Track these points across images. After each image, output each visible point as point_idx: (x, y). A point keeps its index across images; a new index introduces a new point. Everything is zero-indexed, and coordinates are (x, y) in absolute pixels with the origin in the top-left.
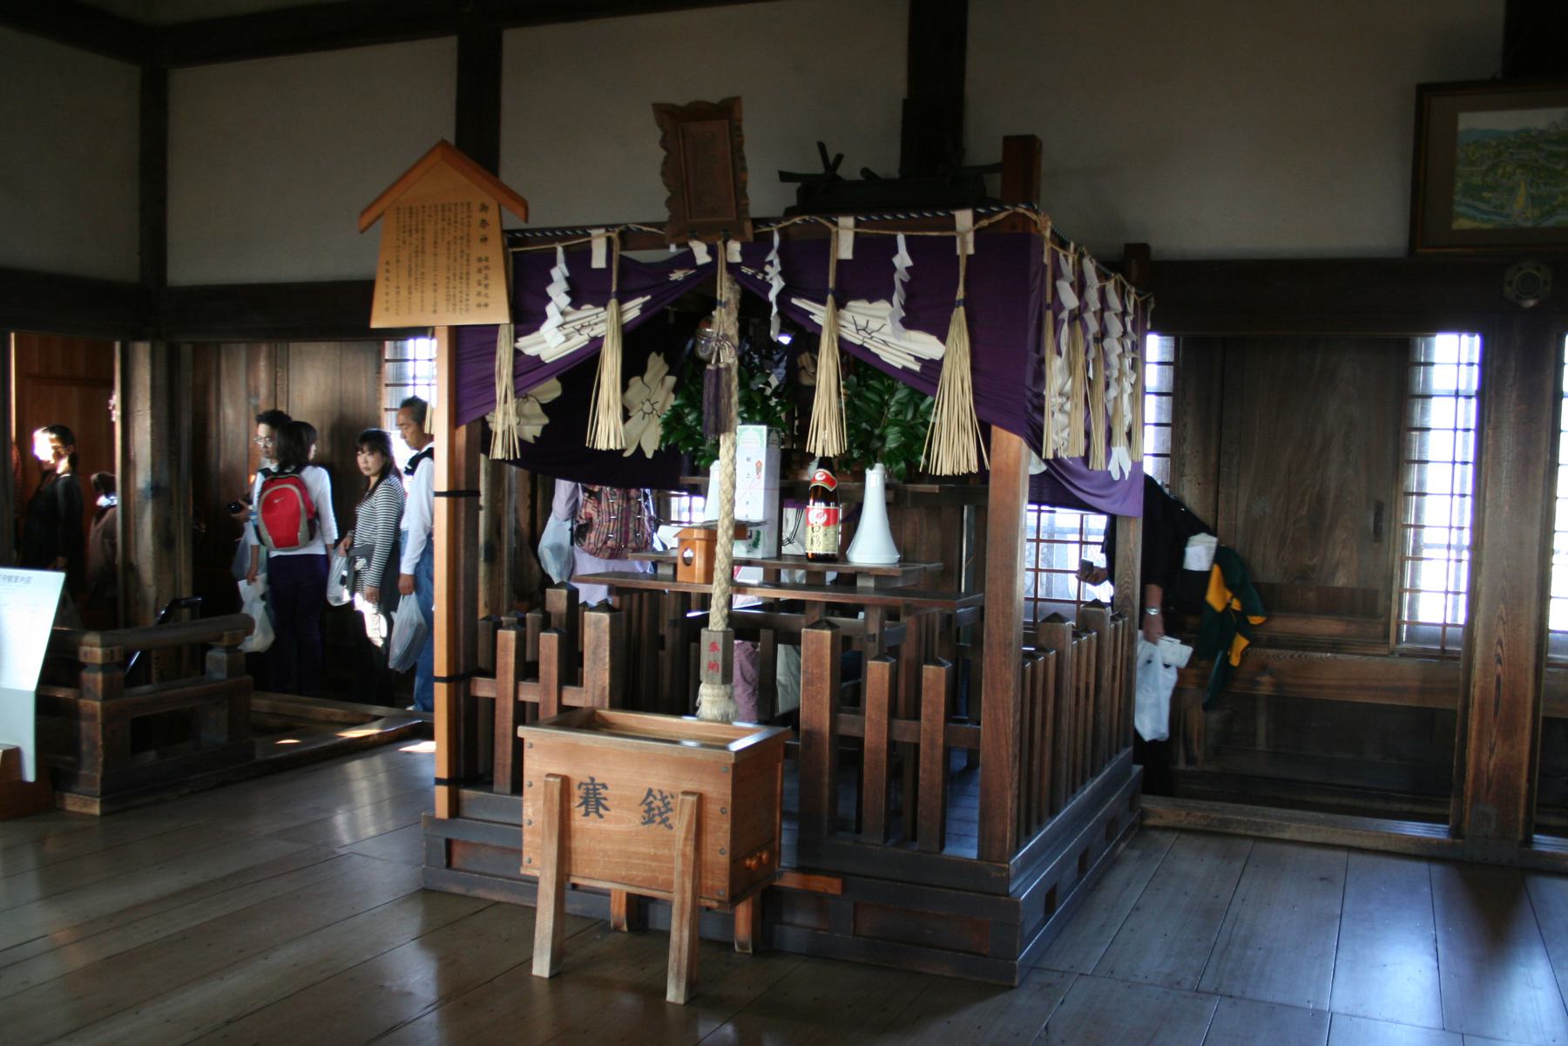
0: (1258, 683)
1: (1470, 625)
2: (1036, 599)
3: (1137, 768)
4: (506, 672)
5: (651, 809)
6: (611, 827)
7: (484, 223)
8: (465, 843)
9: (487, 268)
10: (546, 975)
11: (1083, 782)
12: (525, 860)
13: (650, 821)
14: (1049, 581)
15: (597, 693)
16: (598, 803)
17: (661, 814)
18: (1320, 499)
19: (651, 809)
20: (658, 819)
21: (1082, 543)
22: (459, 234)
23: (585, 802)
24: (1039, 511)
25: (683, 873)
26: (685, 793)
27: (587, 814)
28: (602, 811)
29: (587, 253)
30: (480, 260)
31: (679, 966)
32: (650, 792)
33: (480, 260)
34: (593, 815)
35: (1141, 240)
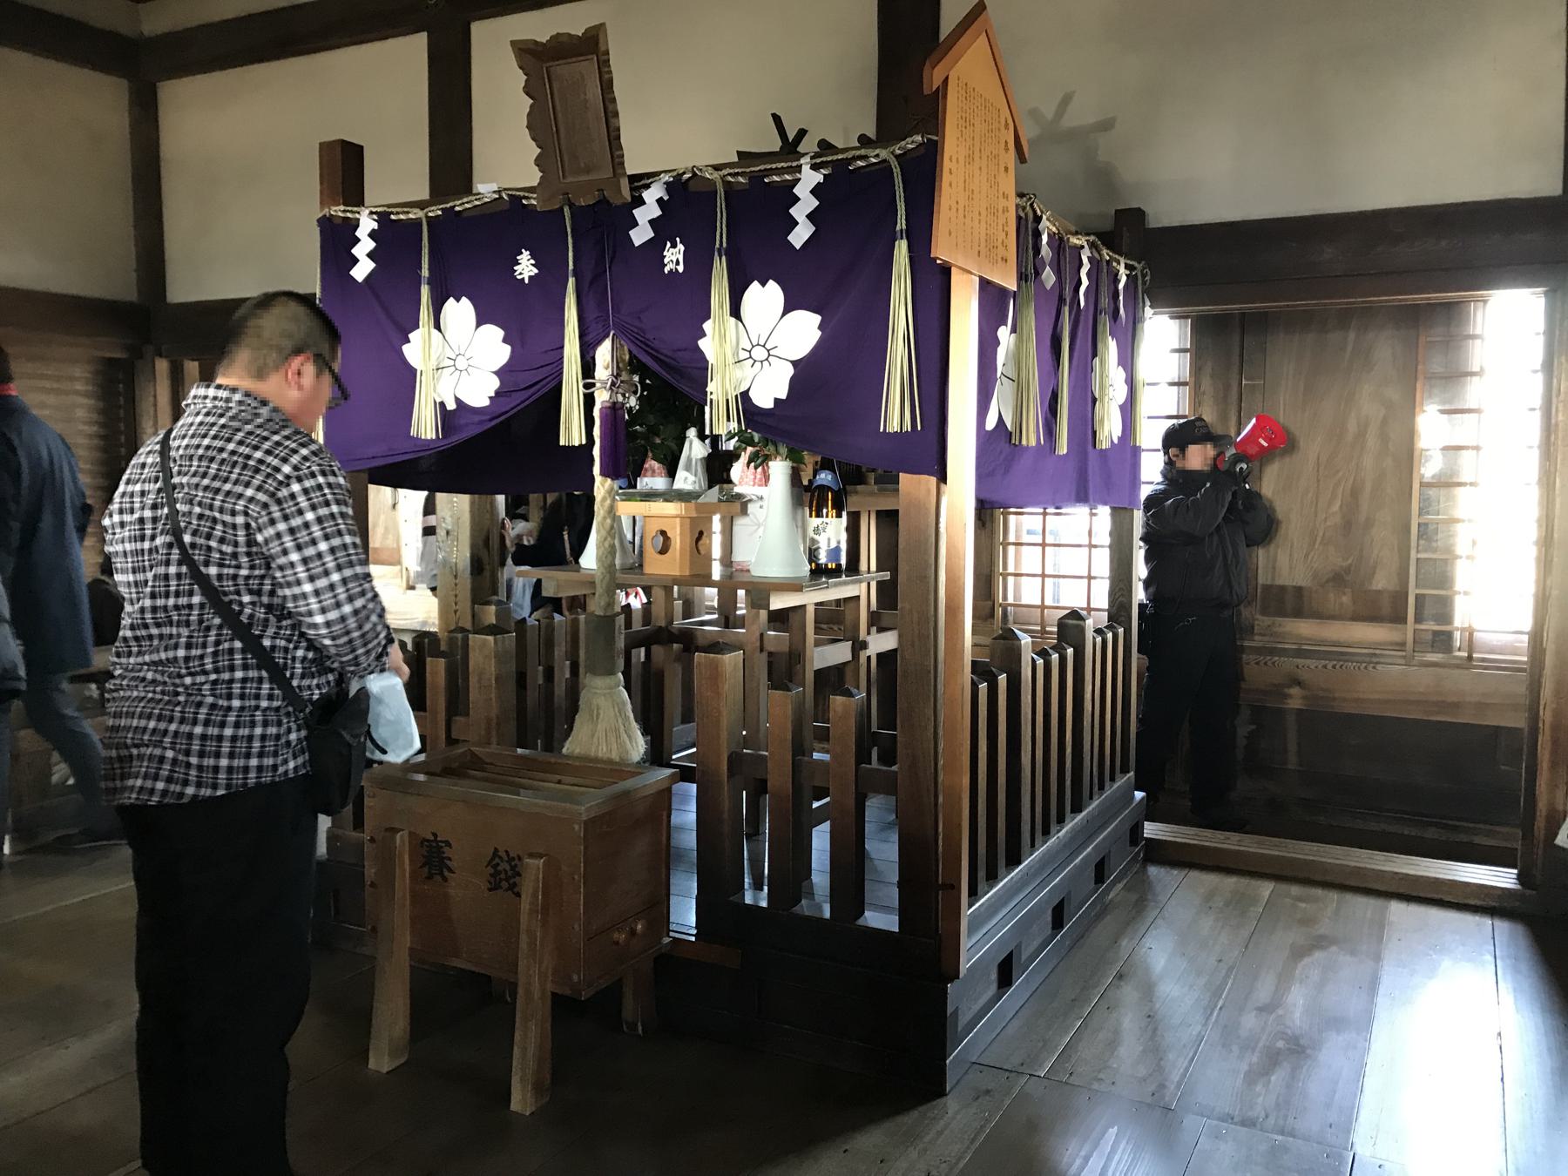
0: (1290, 696)
1: (1536, 637)
2: (1043, 607)
3: (1139, 795)
11: (1061, 820)
14: (1056, 586)
18: (1355, 493)
20: (505, 885)
21: (1091, 546)
24: (1045, 514)
28: (446, 873)
32: (496, 850)
35: (1135, 205)
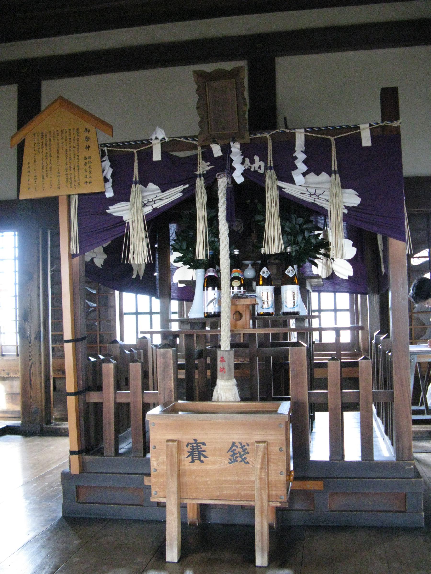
4: (109, 387)
5: (234, 454)
6: (209, 467)
7: (87, 138)
8: (87, 488)
9: (90, 162)
10: (176, 560)
12: (153, 493)
13: (235, 460)
15: (167, 393)
16: (200, 454)
17: (241, 456)
19: (234, 454)
20: (239, 459)
22: (72, 144)
23: (192, 454)
25: (261, 489)
26: (258, 442)
27: (193, 461)
28: (202, 458)
29: (150, 153)
30: (85, 158)
31: (262, 544)
32: (234, 443)
33: (85, 158)
34: (197, 462)
